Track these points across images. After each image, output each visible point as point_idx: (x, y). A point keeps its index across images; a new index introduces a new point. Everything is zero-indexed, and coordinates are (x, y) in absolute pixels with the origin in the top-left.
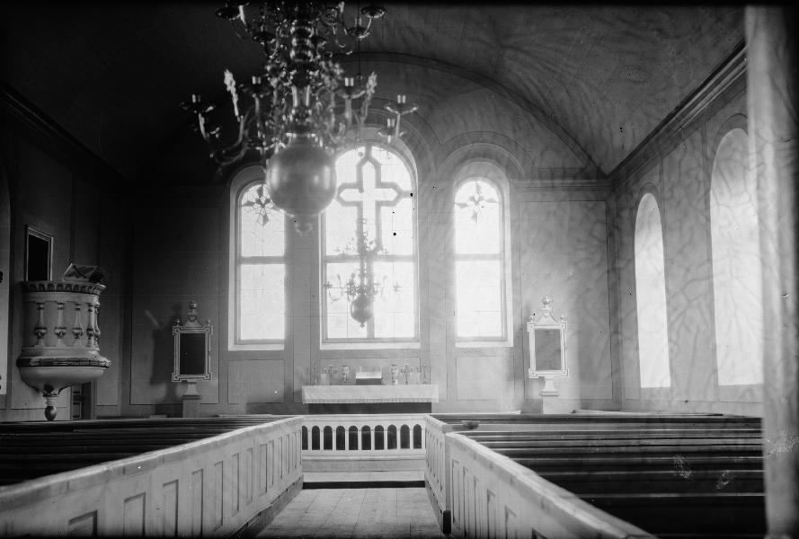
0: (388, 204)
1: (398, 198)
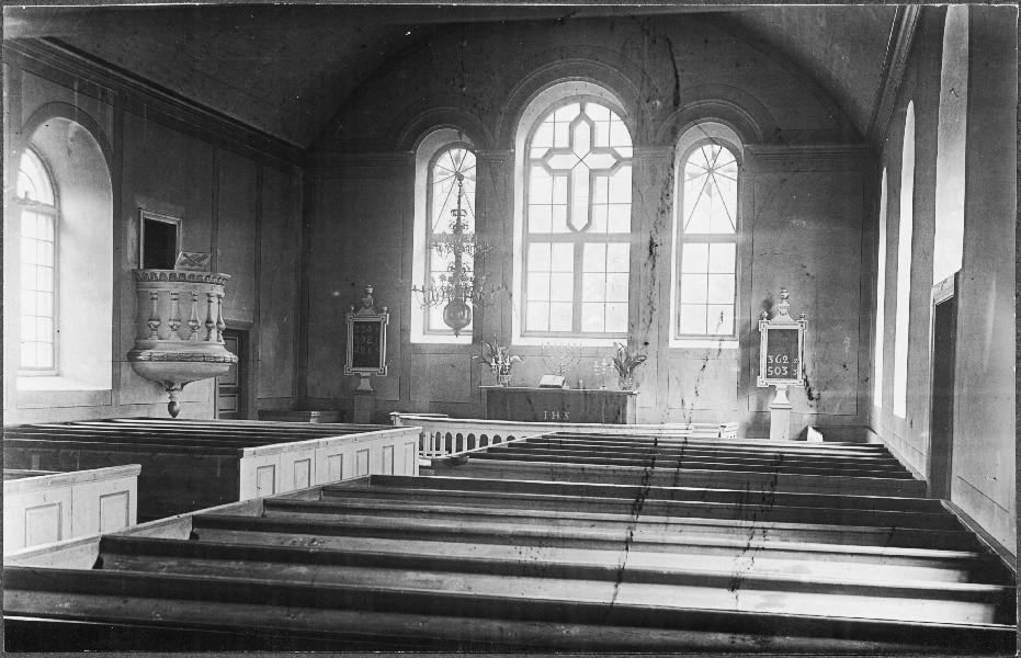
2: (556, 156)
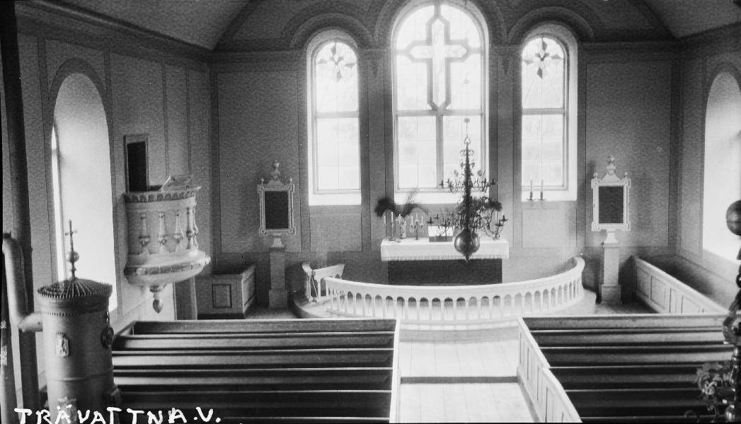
0: (458, 59)
1: (466, 56)
2: (416, 47)
